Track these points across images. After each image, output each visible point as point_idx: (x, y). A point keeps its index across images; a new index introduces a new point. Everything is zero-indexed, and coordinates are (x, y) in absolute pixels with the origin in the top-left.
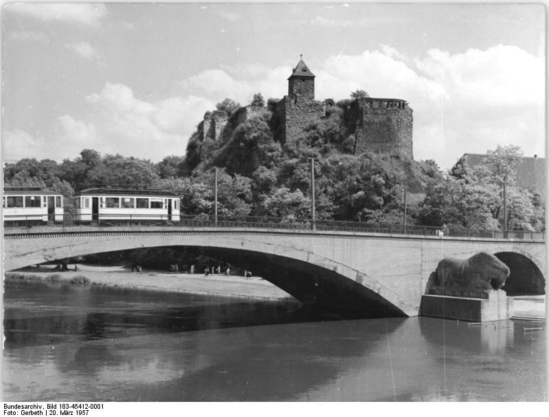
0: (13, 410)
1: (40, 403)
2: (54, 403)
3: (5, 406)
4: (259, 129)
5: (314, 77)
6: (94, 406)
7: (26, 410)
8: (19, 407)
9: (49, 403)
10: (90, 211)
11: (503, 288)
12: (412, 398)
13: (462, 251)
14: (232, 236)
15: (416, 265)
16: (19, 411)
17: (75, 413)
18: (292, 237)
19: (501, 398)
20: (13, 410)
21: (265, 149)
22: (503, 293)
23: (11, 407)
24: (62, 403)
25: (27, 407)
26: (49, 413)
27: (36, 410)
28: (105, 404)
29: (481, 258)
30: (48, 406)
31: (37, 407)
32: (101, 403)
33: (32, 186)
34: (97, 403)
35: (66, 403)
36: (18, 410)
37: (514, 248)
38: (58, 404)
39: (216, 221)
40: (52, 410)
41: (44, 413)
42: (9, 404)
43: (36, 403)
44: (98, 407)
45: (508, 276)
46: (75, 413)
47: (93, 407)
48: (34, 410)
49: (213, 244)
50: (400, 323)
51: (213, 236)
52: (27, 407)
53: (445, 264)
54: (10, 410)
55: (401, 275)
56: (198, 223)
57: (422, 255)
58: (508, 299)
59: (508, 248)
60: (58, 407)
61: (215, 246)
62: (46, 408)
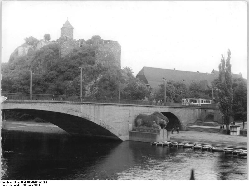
0: (6, 184)
1: (18, 181)
2: (25, 181)
3: (2, 182)
4: (65, 51)
5: (73, 28)
6: (42, 182)
7: (12, 184)
8: (9, 182)
9: (22, 181)
11: (165, 128)
13: (147, 111)
14: (43, 104)
15: (126, 118)
16: (9, 184)
17: (34, 185)
18: (72, 105)
20: (6, 184)
21: (51, 62)
22: (165, 130)
23: (5, 182)
24: (28, 181)
25: (12, 183)
26: (22, 185)
28: (48, 181)
29: (156, 114)
30: (22, 182)
31: (17, 183)
32: (46, 181)
35: (30, 181)
36: (8, 184)
37: (168, 110)
38: (26, 181)
39: (31, 96)
40: (24, 184)
41: (20, 185)
42: (4, 181)
43: (16, 181)
44: (44, 183)
45: (168, 122)
46: (34, 185)
47: (42, 182)
49: (33, 108)
50: (117, 145)
51: (33, 104)
52: (12, 183)
53: (139, 117)
54: (4, 184)
55: (120, 122)
57: (130, 113)
58: (168, 133)
59: (166, 110)
60: (26, 182)
61: (34, 109)
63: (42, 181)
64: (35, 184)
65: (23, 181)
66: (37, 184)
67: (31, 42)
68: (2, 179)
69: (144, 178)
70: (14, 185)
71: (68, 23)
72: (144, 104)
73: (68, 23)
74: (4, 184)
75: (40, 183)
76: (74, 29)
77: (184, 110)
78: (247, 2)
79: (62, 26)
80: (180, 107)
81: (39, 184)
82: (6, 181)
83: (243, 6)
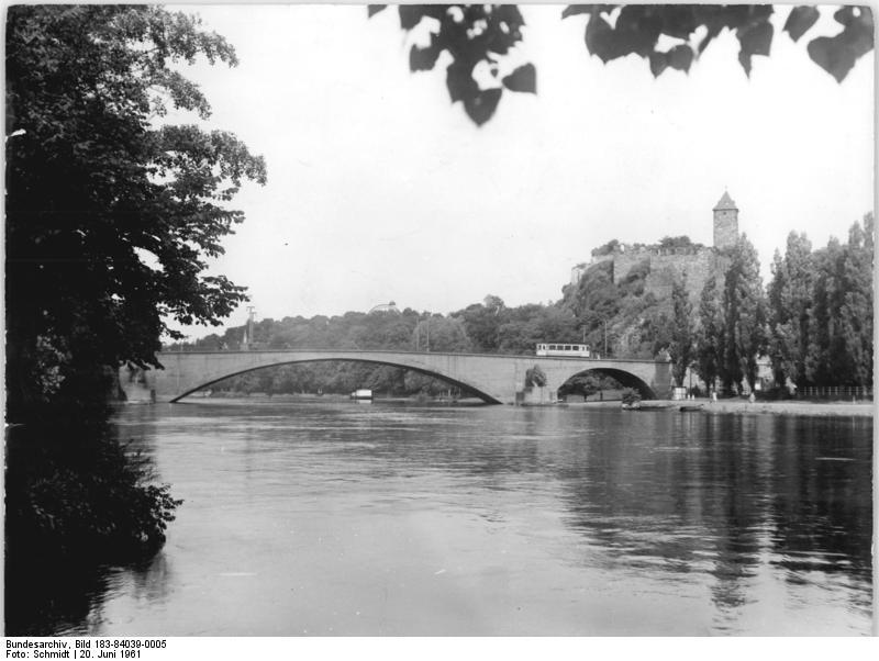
0: (21, 650)
3: (9, 644)
6: (150, 644)
7: (43, 650)
8: (31, 645)
9: (78, 638)
20: (21, 650)
23: (18, 645)
25: (43, 645)
26: (79, 654)
30: (78, 644)
31: (59, 646)
42: (14, 640)
46: (119, 654)
52: (43, 645)
54: (15, 650)
60: (93, 644)
64: (125, 649)
66: (130, 649)
68: (6, 636)
70: (50, 655)
74: (15, 650)
75: (142, 648)
81: (136, 649)
82: (22, 639)
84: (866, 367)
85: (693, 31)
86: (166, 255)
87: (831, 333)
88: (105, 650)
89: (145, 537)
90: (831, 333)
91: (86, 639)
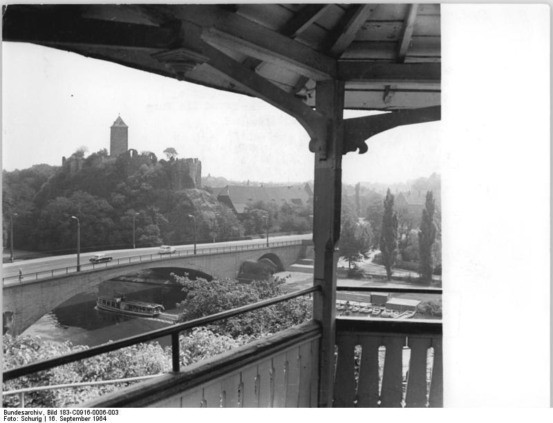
0: (13, 416)
3: (5, 412)
7: (27, 416)
8: (19, 413)
9: (49, 409)
10: (307, 297)
12: (341, 11)
19: (338, 119)
20: (13, 416)
25: (27, 413)
26: (48, 419)
27: (36, 416)
30: (49, 412)
31: (37, 413)
33: (267, 308)
34: (103, 409)
42: (9, 409)
47: (111, 413)
48: (33, 416)
52: (27, 413)
54: (10, 416)
56: (86, 379)
60: (59, 412)
62: (46, 415)
63: (112, 409)
64: (96, 415)
65: (50, 409)
66: (99, 416)
67: (16, 170)
69: (166, 406)
70: (31, 419)
71: (119, 121)
72: (275, 231)
73: (119, 121)
74: (10, 416)
76: (129, 129)
77: (81, 282)
78: (550, 5)
79: (112, 124)
80: (91, 275)
81: (103, 416)
83: (547, 7)
84: (380, 313)
85: (345, 154)
86: (122, 191)
87: (407, 339)
88: (66, 416)
89: (356, 402)
90: (407, 339)
91: (54, 409)
